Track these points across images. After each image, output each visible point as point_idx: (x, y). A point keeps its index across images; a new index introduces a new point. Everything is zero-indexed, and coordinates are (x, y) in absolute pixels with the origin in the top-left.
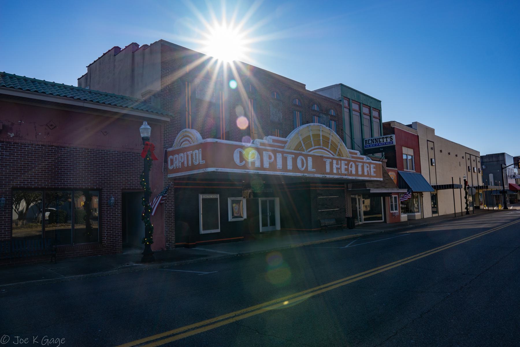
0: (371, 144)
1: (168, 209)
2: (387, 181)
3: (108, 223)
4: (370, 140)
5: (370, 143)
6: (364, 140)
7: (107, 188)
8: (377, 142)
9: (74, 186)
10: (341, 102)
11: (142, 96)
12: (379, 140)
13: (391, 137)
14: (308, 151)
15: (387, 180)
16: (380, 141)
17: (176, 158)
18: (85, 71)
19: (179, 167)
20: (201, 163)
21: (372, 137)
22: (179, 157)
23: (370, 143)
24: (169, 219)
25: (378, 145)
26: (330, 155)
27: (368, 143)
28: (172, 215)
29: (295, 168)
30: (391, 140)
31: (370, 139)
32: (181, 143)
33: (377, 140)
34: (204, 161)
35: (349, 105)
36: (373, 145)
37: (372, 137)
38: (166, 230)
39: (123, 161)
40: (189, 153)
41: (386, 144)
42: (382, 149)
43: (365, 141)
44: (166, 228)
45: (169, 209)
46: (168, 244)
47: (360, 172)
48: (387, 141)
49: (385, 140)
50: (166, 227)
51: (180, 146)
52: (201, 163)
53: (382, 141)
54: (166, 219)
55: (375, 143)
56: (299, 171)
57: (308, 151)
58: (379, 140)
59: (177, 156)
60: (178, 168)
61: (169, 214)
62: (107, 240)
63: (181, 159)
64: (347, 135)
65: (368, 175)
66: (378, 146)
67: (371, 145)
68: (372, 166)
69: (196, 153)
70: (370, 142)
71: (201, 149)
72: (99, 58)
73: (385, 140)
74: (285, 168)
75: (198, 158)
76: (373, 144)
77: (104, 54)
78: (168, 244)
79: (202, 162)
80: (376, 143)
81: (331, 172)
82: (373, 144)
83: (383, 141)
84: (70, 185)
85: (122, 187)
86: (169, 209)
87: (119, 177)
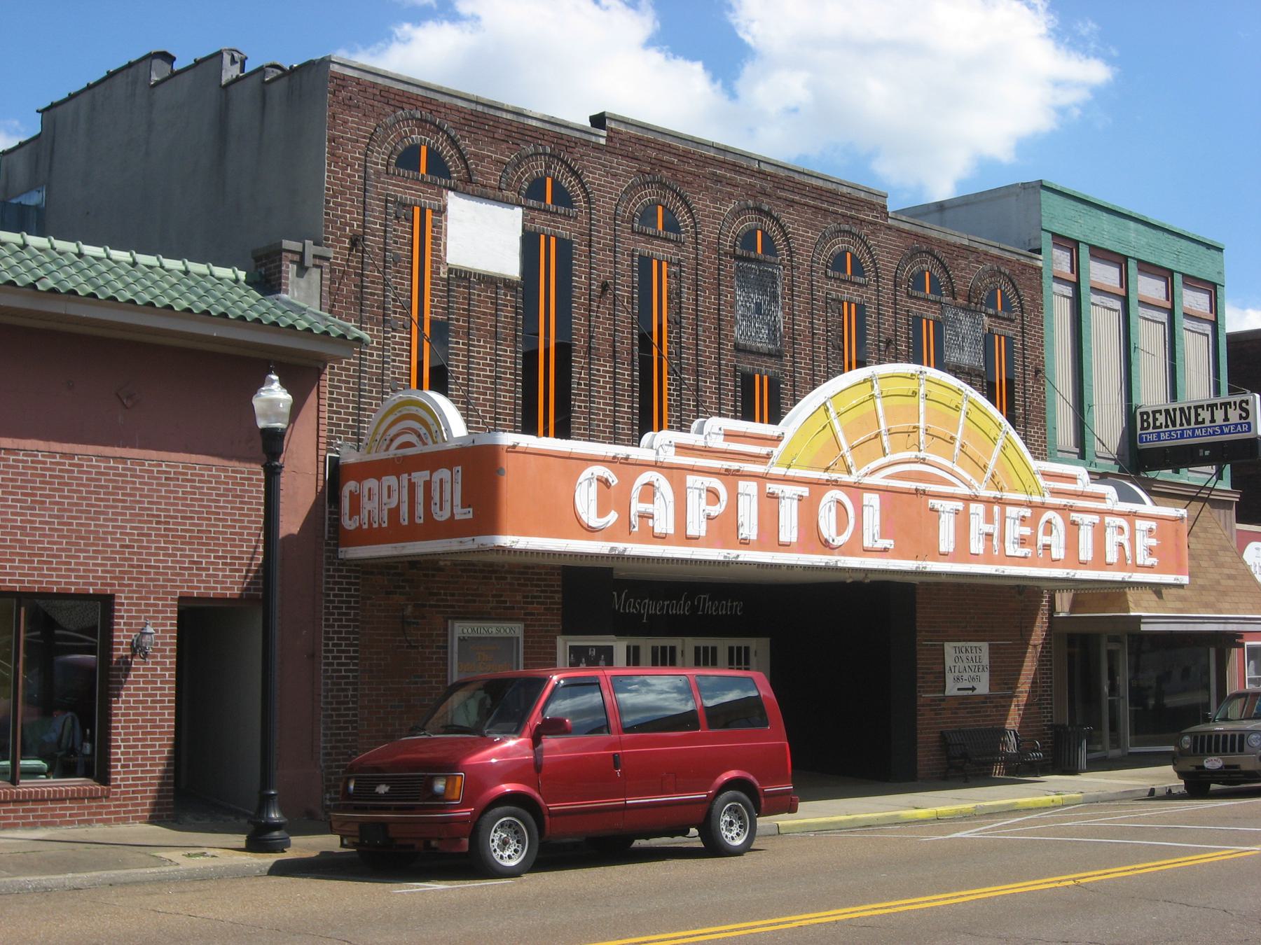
0: (1164, 429)
1: (334, 671)
2: (1231, 583)
3: (128, 715)
4: (1160, 412)
5: (1161, 427)
6: (1139, 411)
7: (130, 592)
8: (1189, 423)
9: (23, 582)
10: (1041, 257)
11: (254, 258)
12: (1197, 415)
13: (1244, 405)
14: (864, 470)
15: (1230, 577)
16: (1200, 419)
17: (370, 489)
18: (33, 127)
19: (380, 524)
20: (457, 517)
21: (1174, 396)
22: (380, 488)
23: (1161, 427)
24: (339, 709)
25: (1193, 437)
26: (956, 486)
27: (1154, 423)
28: (350, 693)
29: (812, 537)
30: (1244, 415)
31: (1163, 408)
32: (392, 440)
33: (1169, 423)
34: (471, 510)
35: (1075, 266)
36: (1170, 435)
37: (1174, 396)
38: (325, 748)
39: (186, 499)
40: (420, 477)
41: (1222, 433)
42: (1207, 453)
43: (1142, 414)
44: (325, 742)
45: (340, 671)
46: (331, 799)
47: (1086, 553)
48: (1226, 419)
49: (1219, 415)
50: (325, 735)
51: (387, 449)
52: (457, 517)
53: (1208, 418)
54: (327, 710)
55: (1182, 424)
56: (826, 546)
57: (864, 470)
58: (1197, 415)
59: (371, 483)
60: (375, 526)
61: (338, 690)
62: (125, 773)
63: (389, 497)
64: (1058, 398)
65: (1122, 564)
66: (1190, 437)
67: (1162, 435)
68: (1142, 525)
69: (441, 480)
70: (1161, 419)
71: (459, 468)
72: (89, 87)
73: (1219, 415)
74: (769, 535)
75: (447, 496)
76: (1171, 428)
77: (111, 75)
78: (331, 799)
79: (463, 514)
80: (1186, 426)
81: (962, 551)
82: (1171, 428)
83: (1213, 420)
84: (10, 581)
85: (178, 591)
86: (340, 671)
87: (102, 487)
